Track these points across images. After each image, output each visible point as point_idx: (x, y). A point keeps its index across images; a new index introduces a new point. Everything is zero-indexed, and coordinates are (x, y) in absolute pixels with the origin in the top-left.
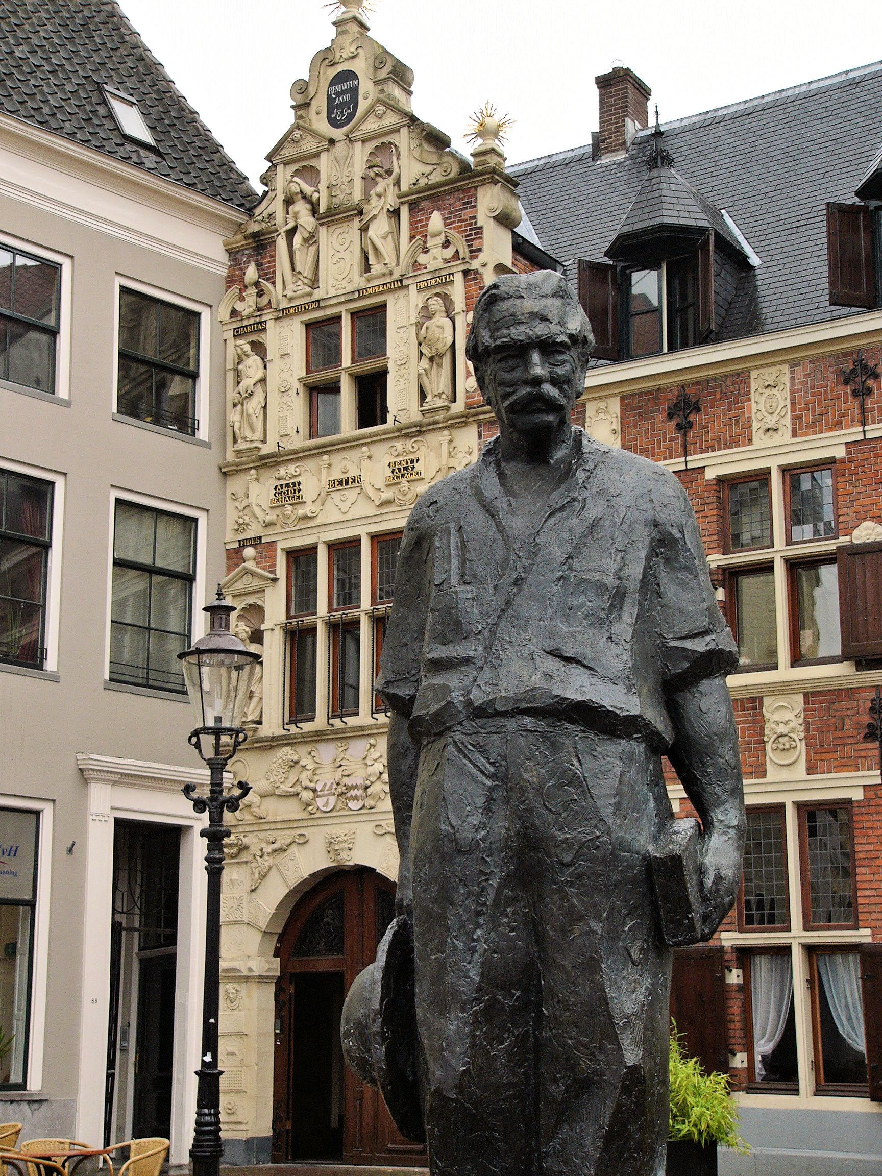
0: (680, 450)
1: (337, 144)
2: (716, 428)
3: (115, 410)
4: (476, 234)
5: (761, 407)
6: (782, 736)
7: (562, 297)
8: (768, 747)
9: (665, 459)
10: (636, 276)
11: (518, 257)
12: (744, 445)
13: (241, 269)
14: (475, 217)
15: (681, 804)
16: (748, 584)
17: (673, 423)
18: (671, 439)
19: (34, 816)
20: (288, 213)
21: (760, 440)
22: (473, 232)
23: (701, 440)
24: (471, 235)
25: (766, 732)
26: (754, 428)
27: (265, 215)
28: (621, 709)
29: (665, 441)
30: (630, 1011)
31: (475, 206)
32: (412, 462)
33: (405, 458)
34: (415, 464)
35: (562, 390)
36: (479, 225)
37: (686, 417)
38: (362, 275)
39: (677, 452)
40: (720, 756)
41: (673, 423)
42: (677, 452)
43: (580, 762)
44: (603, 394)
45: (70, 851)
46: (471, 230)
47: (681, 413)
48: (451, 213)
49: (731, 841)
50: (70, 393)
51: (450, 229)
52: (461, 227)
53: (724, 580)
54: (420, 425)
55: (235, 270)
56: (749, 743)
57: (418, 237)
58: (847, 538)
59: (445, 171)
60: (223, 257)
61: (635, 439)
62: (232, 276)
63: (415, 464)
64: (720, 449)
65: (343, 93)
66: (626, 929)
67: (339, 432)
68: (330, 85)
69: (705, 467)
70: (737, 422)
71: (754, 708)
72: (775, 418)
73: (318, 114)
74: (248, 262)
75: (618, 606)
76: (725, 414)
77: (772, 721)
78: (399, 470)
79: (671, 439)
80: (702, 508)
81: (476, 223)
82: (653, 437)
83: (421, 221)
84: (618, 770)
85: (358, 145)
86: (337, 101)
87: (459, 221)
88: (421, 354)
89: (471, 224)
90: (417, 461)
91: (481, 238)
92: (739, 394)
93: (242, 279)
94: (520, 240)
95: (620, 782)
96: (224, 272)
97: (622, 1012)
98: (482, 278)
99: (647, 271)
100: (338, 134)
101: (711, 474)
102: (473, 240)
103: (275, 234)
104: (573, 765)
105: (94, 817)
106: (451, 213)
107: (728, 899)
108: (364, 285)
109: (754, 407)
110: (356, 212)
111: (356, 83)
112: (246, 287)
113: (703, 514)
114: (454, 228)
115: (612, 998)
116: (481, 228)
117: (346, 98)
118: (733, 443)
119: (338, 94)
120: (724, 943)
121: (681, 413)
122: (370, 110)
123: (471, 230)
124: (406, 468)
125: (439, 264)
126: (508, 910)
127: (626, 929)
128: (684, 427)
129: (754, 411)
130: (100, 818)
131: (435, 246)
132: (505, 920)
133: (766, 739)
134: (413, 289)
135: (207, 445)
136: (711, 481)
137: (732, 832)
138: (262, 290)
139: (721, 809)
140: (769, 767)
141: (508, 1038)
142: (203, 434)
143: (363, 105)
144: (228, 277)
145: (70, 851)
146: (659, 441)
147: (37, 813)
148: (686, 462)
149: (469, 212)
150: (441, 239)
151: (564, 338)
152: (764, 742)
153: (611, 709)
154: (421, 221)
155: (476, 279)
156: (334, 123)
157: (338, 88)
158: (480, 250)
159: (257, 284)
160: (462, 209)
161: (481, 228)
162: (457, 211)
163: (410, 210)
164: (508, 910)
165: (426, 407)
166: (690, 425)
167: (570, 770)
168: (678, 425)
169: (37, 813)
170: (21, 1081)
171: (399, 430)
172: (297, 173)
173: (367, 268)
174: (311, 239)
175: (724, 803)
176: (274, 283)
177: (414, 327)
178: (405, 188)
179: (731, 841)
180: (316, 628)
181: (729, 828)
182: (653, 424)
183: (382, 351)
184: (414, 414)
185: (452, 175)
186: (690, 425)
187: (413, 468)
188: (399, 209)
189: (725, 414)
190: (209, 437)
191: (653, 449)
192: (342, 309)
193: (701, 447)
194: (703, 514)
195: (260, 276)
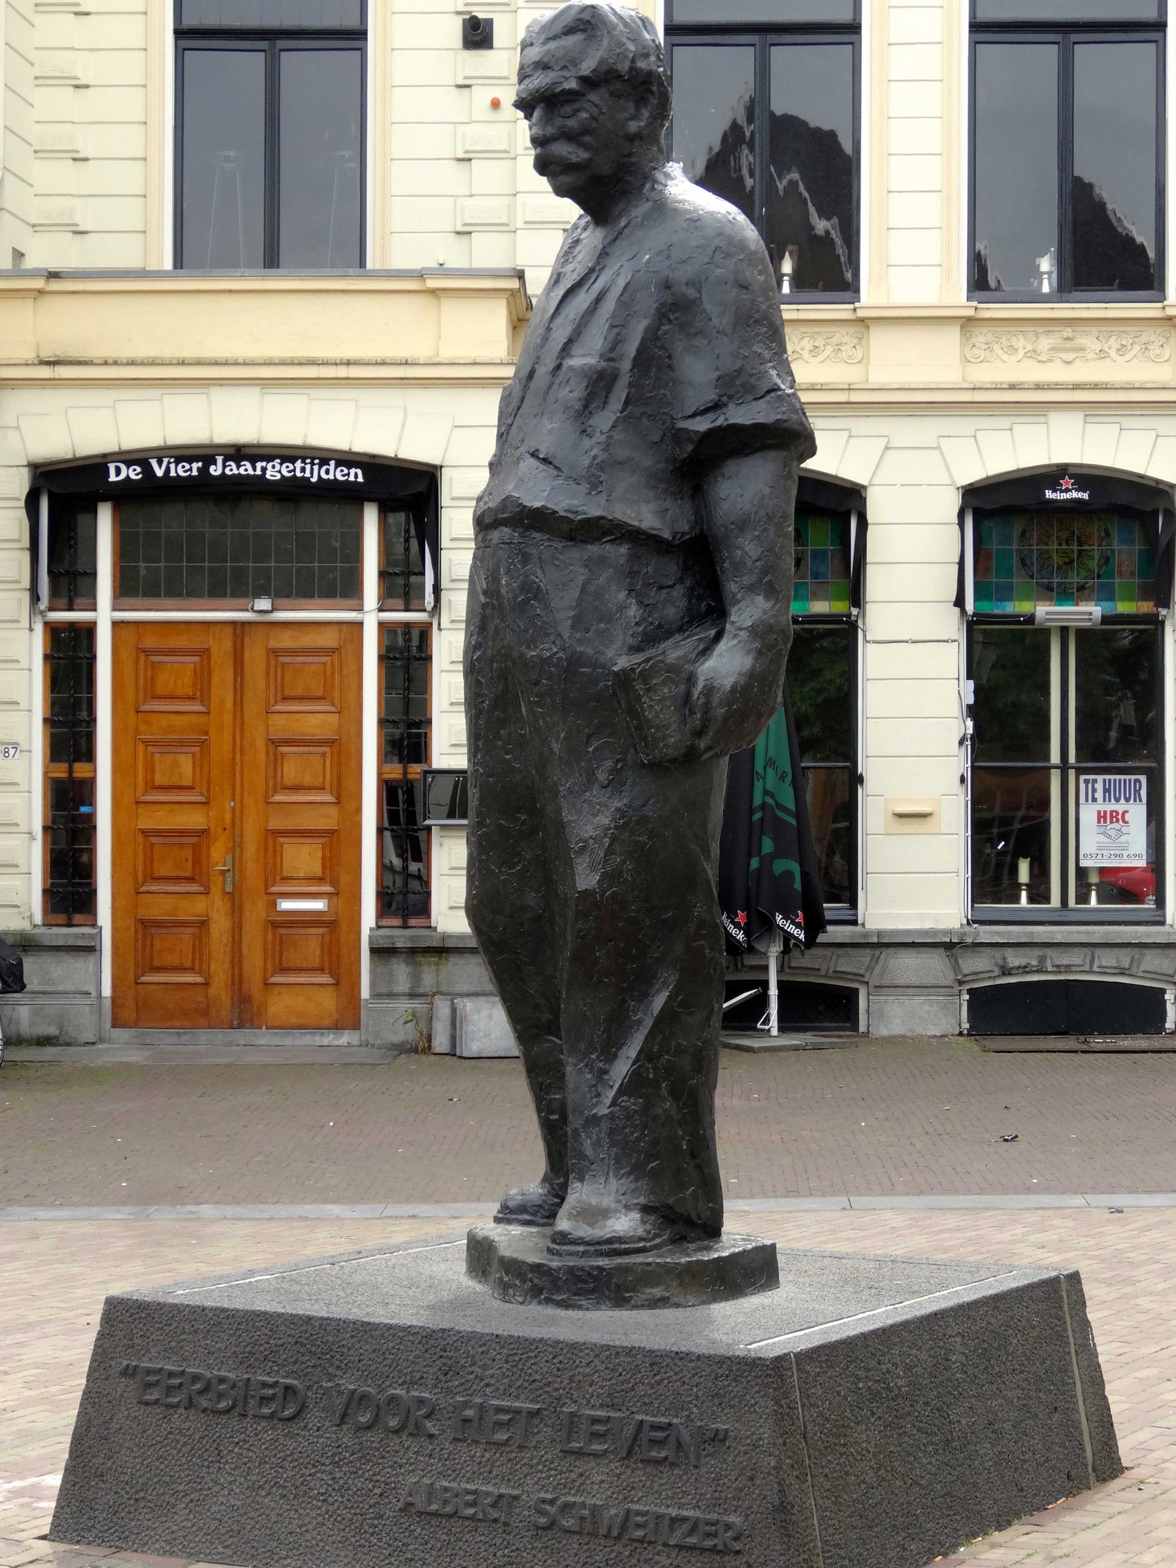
7: (584, 31)
28: (577, 512)
30: (587, 835)
35: (580, 144)
40: (738, 548)
43: (544, 572)
49: (741, 645)
58: (786, 278)
66: (591, 749)
75: (603, 394)
84: (580, 580)
95: (582, 592)
97: (578, 835)
104: (537, 577)
107: (723, 711)
115: (570, 822)
126: (502, 732)
127: (591, 749)
132: (499, 743)
137: (743, 635)
139: (736, 608)
141: (519, 862)
151: (572, 84)
153: (563, 514)
164: (502, 732)
167: (535, 583)
170: (1142, 863)
175: (739, 601)
179: (741, 645)
181: (741, 629)
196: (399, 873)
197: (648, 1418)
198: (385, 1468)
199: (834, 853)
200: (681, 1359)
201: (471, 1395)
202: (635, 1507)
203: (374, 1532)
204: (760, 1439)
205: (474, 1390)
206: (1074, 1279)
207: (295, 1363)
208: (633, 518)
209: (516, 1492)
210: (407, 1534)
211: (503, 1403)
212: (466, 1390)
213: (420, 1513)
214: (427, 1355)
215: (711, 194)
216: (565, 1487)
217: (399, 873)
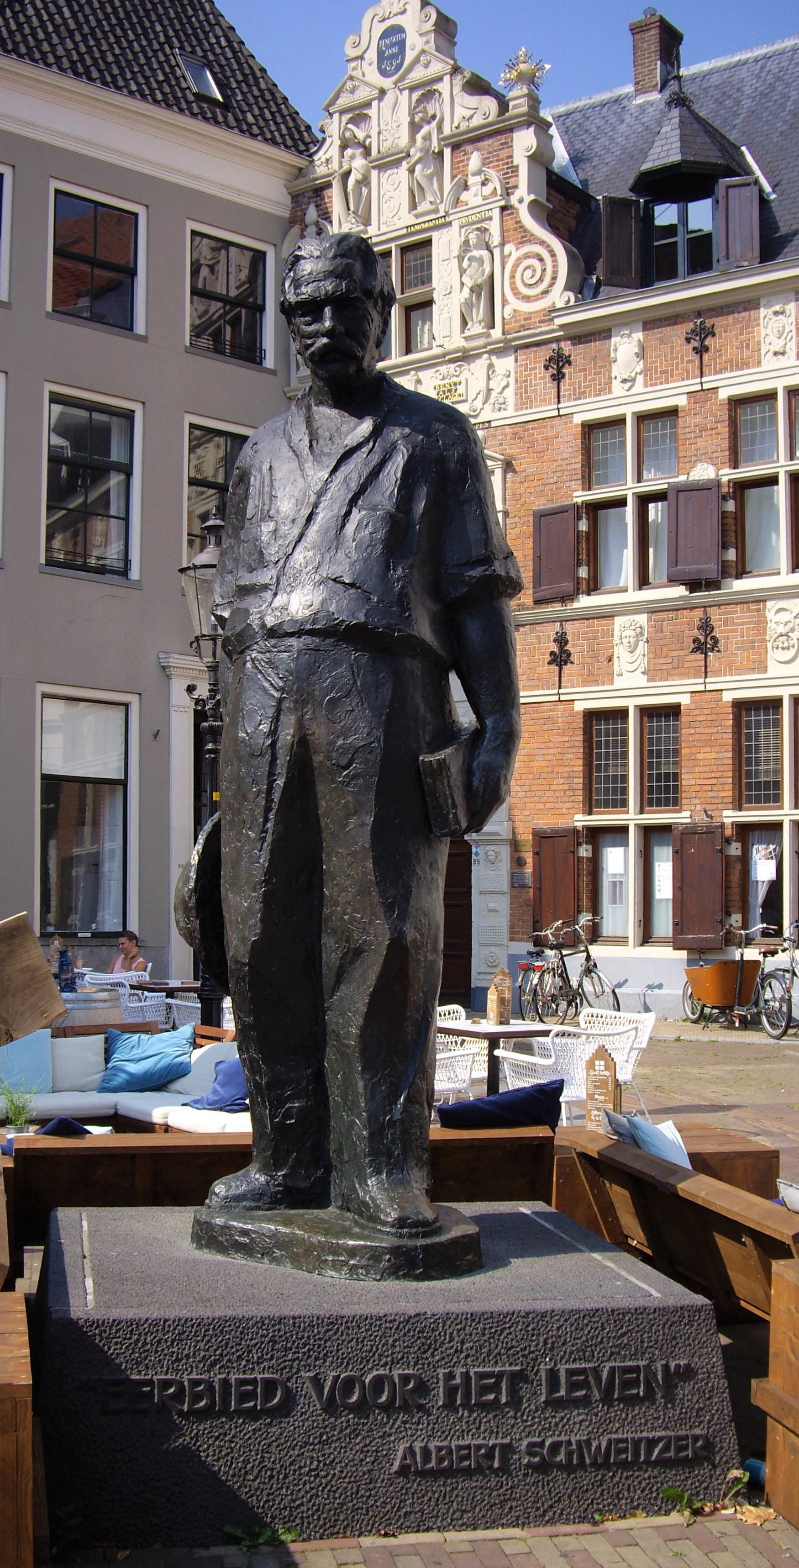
0: (697, 372)
1: (389, 93)
2: (730, 352)
3: (49, 308)
4: (512, 172)
5: (769, 331)
6: (781, 635)
8: (769, 645)
9: (683, 380)
10: (658, 209)
11: (553, 192)
12: (754, 367)
13: (302, 210)
14: (511, 157)
15: (691, 697)
16: (753, 494)
17: (690, 346)
18: (689, 362)
19: (124, 707)
20: (343, 157)
21: (769, 363)
22: (510, 171)
23: (715, 363)
24: (508, 173)
25: (768, 632)
26: (763, 352)
27: (323, 159)
29: (682, 363)
31: (512, 146)
32: (455, 384)
33: (450, 381)
34: (458, 387)
36: (515, 163)
37: (702, 341)
38: (410, 213)
39: (693, 373)
41: (690, 346)
42: (693, 373)
44: (626, 320)
45: (156, 736)
46: (507, 168)
47: (698, 338)
48: (490, 153)
50: (147, 328)
51: (489, 168)
52: (498, 166)
53: (734, 492)
54: (465, 350)
55: (296, 211)
56: (753, 642)
57: (459, 176)
59: (485, 115)
60: (288, 200)
61: (656, 362)
62: (294, 216)
63: (458, 387)
64: (732, 370)
65: (393, 45)
67: (612, 684)
68: (381, 38)
69: (717, 388)
70: (748, 346)
71: (758, 610)
72: (782, 342)
73: (370, 65)
74: (309, 204)
76: (737, 339)
77: (773, 622)
78: (444, 392)
79: (689, 362)
80: (715, 426)
81: (512, 162)
82: (672, 359)
83: (462, 161)
85: (406, 93)
86: (387, 53)
87: (497, 161)
88: (462, 284)
89: (508, 163)
90: (460, 384)
91: (517, 176)
92: (750, 319)
93: (303, 220)
94: (554, 177)
96: (286, 214)
98: (518, 213)
99: (668, 205)
100: (387, 83)
101: (724, 394)
102: (509, 178)
103: (331, 178)
105: (176, 709)
106: (490, 153)
108: (412, 220)
109: (763, 333)
110: (404, 154)
111: (404, 36)
112: (307, 226)
113: (717, 431)
114: (493, 167)
116: (517, 167)
117: (395, 50)
118: (745, 365)
119: (388, 47)
120: (726, 820)
121: (698, 338)
122: (416, 61)
123: (507, 168)
124: (450, 391)
125: (479, 201)
128: (701, 350)
129: (763, 335)
130: (181, 709)
131: (475, 184)
133: (767, 638)
134: (456, 225)
135: (272, 372)
136: (724, 400)
138: (321, 229)
140: (771, 664)
142: (269, 362)
143: (410, 56)
144: (291, 218)
145: (156, 736)
146: (677, 363)
147: (127, 705)
148: (701, 383)
149: (503, 154)
150: (479, 179)
152: (766, 641)
154: (462, 161)
155: (512, 213)
156: (383, 73)
157: (388, 41)
158: (516, 187)
159: (317, 224)
160: (500, 150)
161: (517, 167)
162: (495, 151)
163: (452, 151)
165: (467, 333)
166: (707, 349)
168: (694, 349)
169: (127, 705)
171: (444, 355)
172: (351, 121)
173: (413, 206)
174: (365, 181)
176: (331, 222)
177: (456, 259)
178: (447, 131)
180: (211, 1025)
182: (672, 348)
183: (427, 279)
184: (457, 342)
185: (491, 119)
186: (707, 349)
187: (456, 390)
188: (443, 151)
189: (737, 339)
190: (275, 366)
191: (672, 370)
192: (393, 245)
193: (737, 366)
194: (717, 431)
195: (319, 216)
196: (309, 143)
197: (618, 1364)
198: (375, 1439)
199: (327, 1260)
200: (641, 1313)
201: (454, 1366)
202: (614, 1436)
203: (370, 1495)
204: (713, 1367)
205: (455, 1363)
206: (14, 1290)
207: (272, 1358)
208: (544, 504)
209: (507, 1441)
210: (404, 1491)
211: (485, 1369)
212: (446, 1363)
213: (418, 1473)
214: (407, 1339)
215: (462, 688)
216: (549, 1430)
217: (309, 143)
